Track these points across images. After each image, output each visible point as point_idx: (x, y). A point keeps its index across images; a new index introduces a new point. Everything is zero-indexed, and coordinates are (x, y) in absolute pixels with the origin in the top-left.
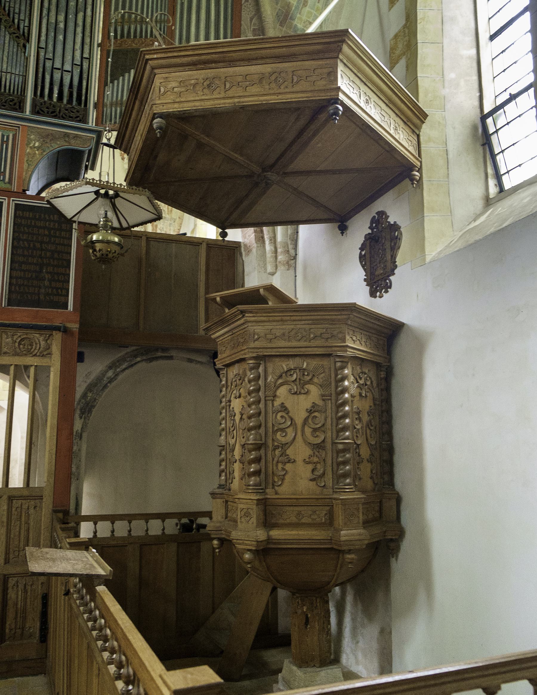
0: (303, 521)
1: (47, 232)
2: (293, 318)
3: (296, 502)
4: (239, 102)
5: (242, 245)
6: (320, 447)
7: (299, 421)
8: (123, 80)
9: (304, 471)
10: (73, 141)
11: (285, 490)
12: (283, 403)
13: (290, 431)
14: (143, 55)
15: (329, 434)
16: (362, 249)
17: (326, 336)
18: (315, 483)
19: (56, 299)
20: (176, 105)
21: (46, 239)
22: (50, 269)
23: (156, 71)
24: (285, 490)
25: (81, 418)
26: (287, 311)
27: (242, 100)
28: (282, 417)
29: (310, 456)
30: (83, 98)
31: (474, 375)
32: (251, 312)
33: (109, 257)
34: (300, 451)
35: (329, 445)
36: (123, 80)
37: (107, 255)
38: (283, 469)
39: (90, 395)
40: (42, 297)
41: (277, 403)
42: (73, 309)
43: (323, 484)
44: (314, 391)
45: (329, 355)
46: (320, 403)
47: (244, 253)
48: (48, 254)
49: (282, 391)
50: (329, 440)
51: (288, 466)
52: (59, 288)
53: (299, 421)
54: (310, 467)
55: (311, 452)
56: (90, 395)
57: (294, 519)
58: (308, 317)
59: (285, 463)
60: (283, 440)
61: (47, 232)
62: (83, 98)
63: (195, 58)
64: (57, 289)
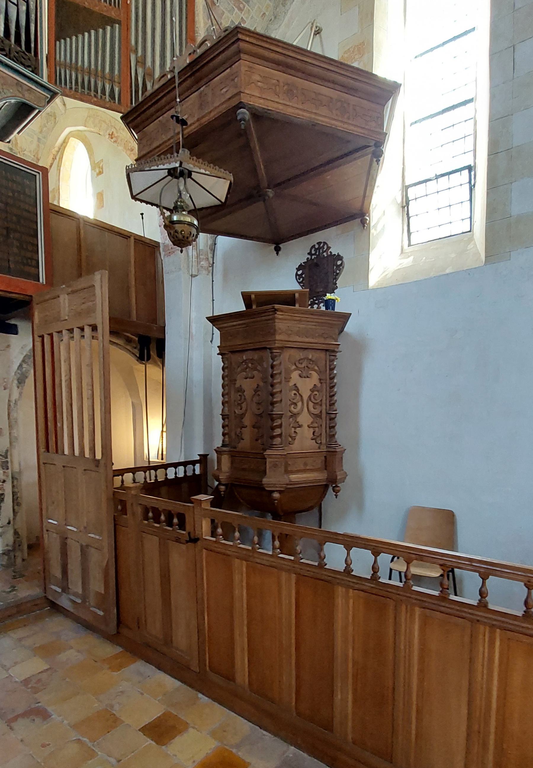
0: (308, 468)
1: (11, 194)
2: (308, 319)
3: (303, 455)
4: (314, 118)
5: (161, 245)
6: (319, 416)
7: (305, 398)
8: (65, 43)
9: (308, 433)
10: (27, 95)
11: (296, 447)
12: (295, 384)
13: (299, 404)
14: (236, 32)
15: (324, 407)
16: (298, 269)
17: (326, 336)
18: (314, 441)
19: (27, 269)
20: (262, 101)
21: (10, 201)
22: (17, 235)
23: (242, 55)
24: (296, 447)
25: (18, 387)
26: (306, 314)
27: (317, 117)
28: (295, 394)
29: (312, 423)
30: (33, 45)
31: (411, 371)
32: (282, 311)
33: (189, 240)
34: (305, 419)
35: (324, 415)
36: (65, 43)
37: (188, 238)
38: (295, 432)
39: (25, 366)
40: (12, 266)
41: (291, 384)
42: (46, 282)
43: (320, 442)
44: (315, 376)
45: (265, 348)
46: (319, 385)
47: (163, 254)
48: (14, 218)
49: (295, 375)
50: (324, 412)
51: (298, 430)
52: (29, 258)
53: (305, 398)
54: (312, 430)
55: (312, 420)
56: (25, 366)
57: (302, 467)
58: (316, 320)
59: (295, 428)
60: (295, 411)
61: (11, 194)
62: (33, 45)
63: (281, 58)
64: (28, 258)
